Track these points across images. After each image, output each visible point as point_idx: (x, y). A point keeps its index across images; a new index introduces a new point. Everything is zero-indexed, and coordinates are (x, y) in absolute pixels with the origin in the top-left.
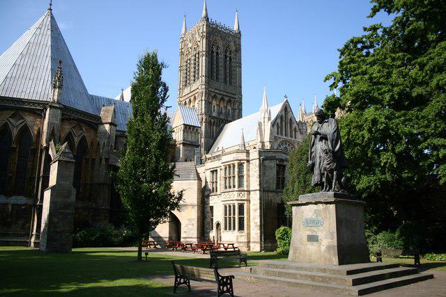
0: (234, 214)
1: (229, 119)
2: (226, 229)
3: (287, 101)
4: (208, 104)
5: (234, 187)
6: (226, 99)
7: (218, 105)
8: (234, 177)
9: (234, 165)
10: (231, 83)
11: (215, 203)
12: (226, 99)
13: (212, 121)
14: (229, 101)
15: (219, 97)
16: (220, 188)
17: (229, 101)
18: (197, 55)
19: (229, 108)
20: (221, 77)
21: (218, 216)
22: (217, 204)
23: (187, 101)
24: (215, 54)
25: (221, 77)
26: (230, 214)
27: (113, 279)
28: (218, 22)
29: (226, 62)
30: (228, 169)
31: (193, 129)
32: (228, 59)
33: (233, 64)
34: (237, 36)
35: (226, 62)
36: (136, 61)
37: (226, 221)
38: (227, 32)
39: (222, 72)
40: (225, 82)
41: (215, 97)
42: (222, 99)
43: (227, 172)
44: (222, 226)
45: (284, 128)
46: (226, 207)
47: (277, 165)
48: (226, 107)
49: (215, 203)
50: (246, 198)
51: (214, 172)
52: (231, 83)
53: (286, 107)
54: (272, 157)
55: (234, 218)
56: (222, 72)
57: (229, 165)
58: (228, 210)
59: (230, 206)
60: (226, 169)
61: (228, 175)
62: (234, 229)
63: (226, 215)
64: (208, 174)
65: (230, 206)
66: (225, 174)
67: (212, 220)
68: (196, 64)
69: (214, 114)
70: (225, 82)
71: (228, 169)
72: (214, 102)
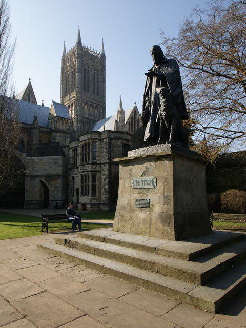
0: (89, 183)
1: (97, 120)
2: (82, 194)
3: (136, 106)
4: (82, 108)
5: (89, 161)
6: (95, 105)
7: (89, 109)
8: (89, 153)
9: (89, 143)
10: (98, 94)
11: (76, 174)
12: (95, 105)
13: (85, 120)
14: (97, 107)
15: (89, 103)
16: (79, 162)
17: (97, 107)
18: (73, 72)
19: (96, 112)
20: (92, 88)
21: (78, 184)
22: (77, 175)
23: (70, 104)
24: (86, 72)
25: (92, 88)
26: (86, 183)
27: (89, 219)
28: (89, 47)
29: (94, 78)
30: (84, 147)
31: (64, 120)
32: (96, 76)
33: (100, 80)
34: (103, 58)
35: (94, 78)
36: (238, 316)
37: (82, 187)
38: (96, 55)
39: (92, 85)
40: (94, 93)
41: (86, 103)
42: (92, 105)
43: (84, 149)
44: (80, 192)
45: (133, 126)
46: (82, 176)
47: (123, 144)
48: (94, 111)
49: (76, 174)
50: (97, 169)
51: (75, 150)
52: (98, 94)
53: (135, 111)
54: (119, 137)
55: (89, 185)
56: (92, 85)
57: (86, 144)
58: (84, 179)
59: (86, 176)
60: (83, 146)
61: (84, 151)
62: (89, 194)
63: (82, 182)
64: (71, 151)
65: (86, 176)
66: (83, 151)
67: (74, 187)
68: (73, 78)
69: (86, 116)
70: (94, 93)
71: (84, 147)
72: (86, 107)
